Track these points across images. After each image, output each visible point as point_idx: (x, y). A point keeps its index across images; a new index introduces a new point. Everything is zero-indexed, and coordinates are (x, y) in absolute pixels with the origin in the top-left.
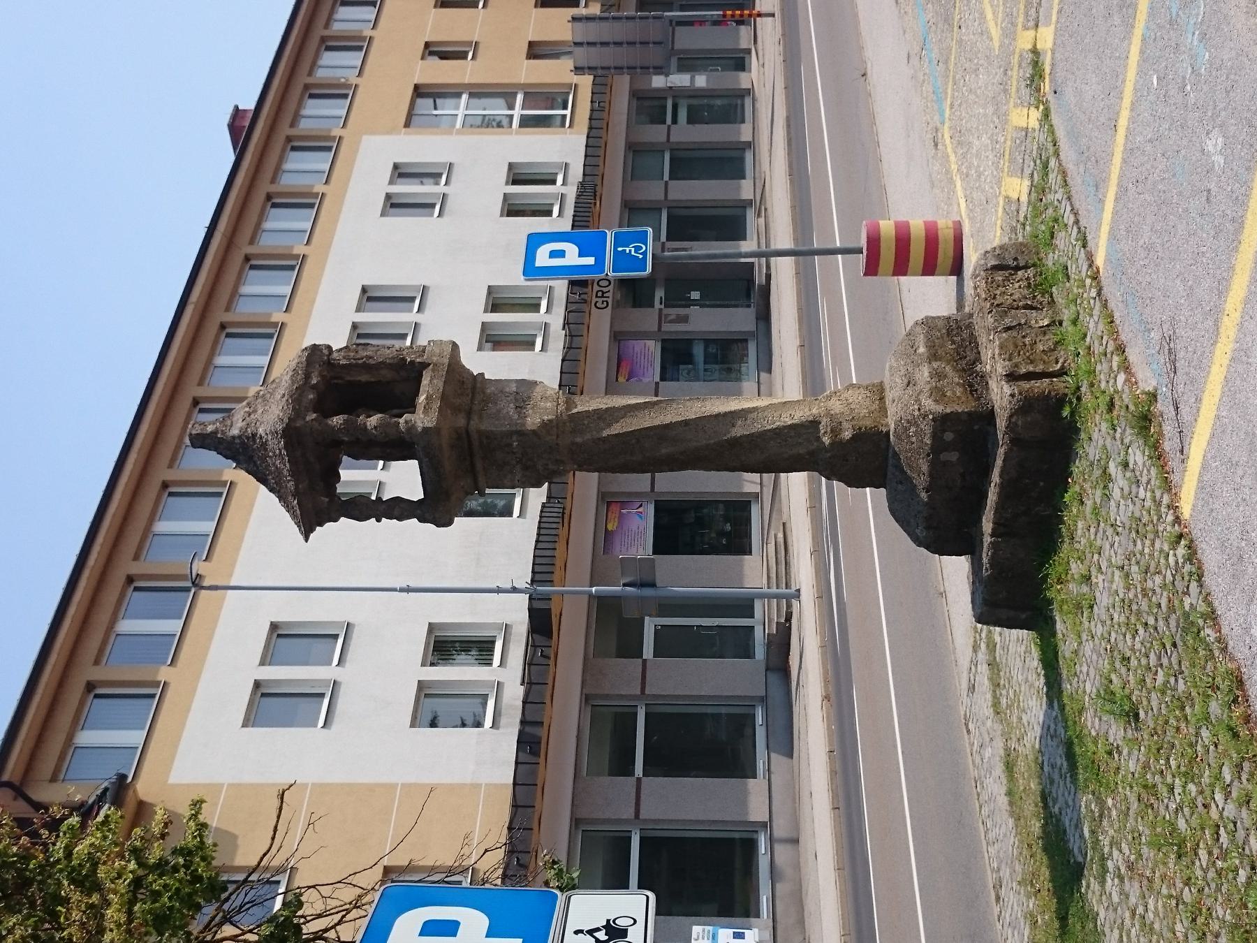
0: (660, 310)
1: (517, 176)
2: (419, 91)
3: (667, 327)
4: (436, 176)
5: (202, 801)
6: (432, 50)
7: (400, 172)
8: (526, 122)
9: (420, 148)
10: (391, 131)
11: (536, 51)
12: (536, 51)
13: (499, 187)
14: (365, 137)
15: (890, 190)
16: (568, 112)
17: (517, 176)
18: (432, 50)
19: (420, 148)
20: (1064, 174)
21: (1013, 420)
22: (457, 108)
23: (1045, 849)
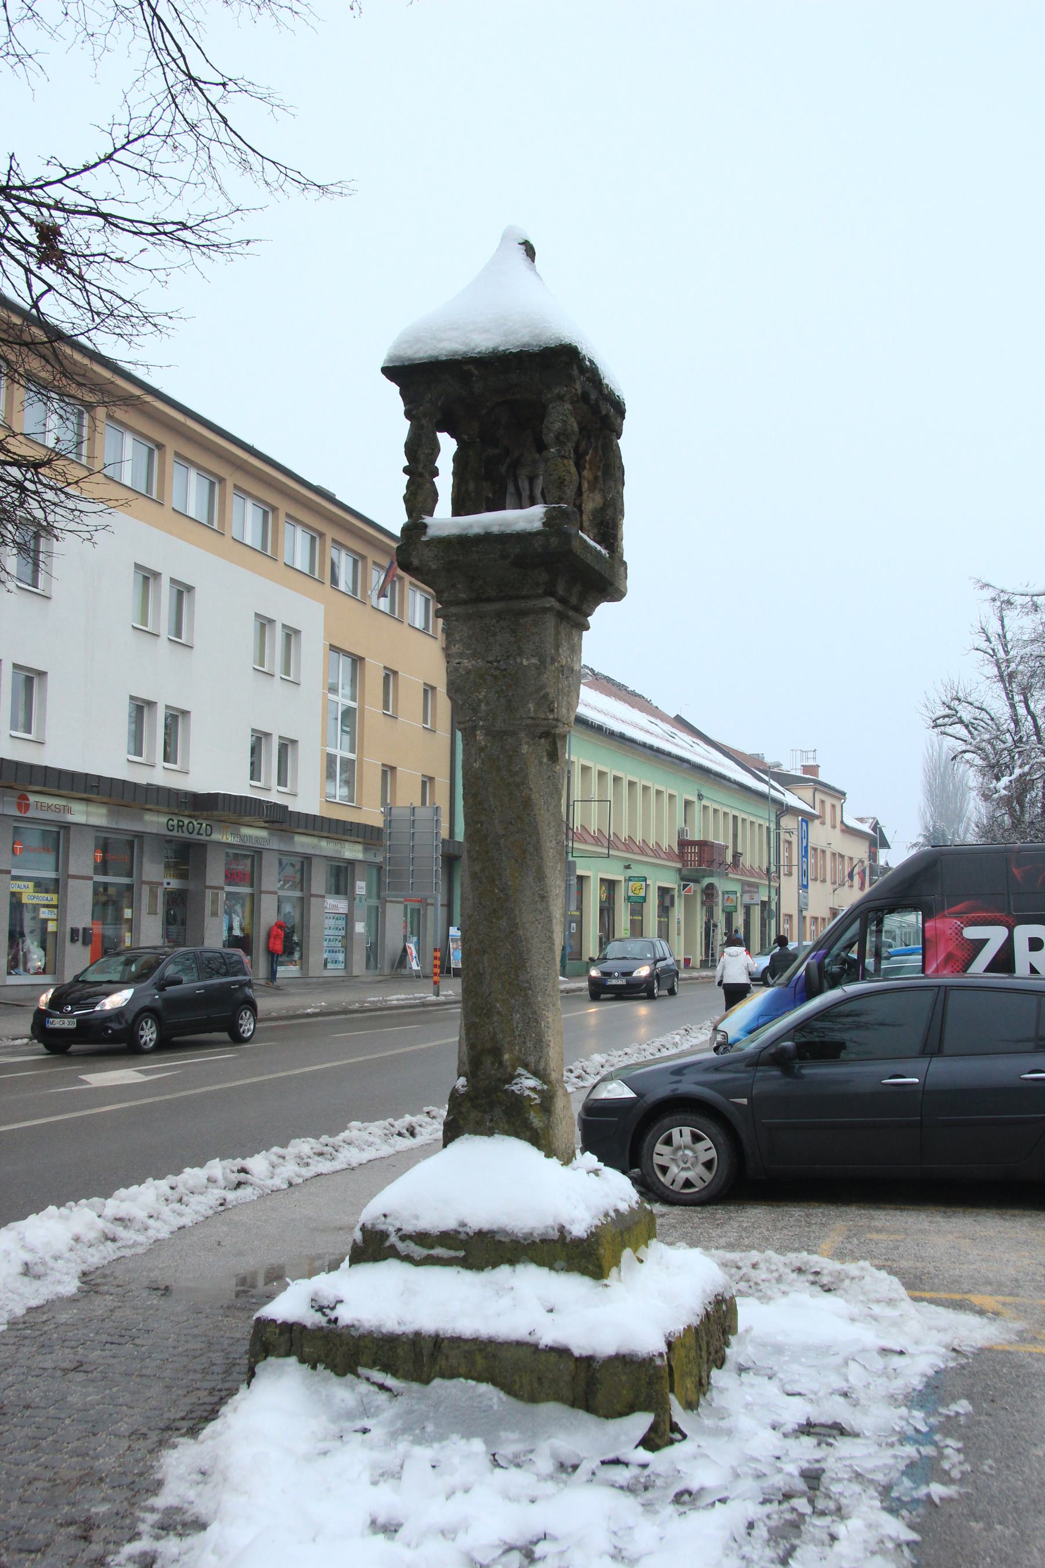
0: (162, 884)
1: (286, 746)
2: (357, 661)
3: (146, 889)
4: (287, 671)
5: (341, 1301)
6: (390, 675)
7: (291, 634)
8: (331, 759)
9: (312, 650)
10: (328, 632)
11: (389, 771)
12: (389, 771)
13: (278, 730)
14: (322, 607)
15: (443, 1228)
16: (337, 800)
17: (286, 746)
18: (390, 675)
19: (312, 650)
20: (112, 292)
21: (503, 923)
22: (344, 696)
23: (107, 1195)
